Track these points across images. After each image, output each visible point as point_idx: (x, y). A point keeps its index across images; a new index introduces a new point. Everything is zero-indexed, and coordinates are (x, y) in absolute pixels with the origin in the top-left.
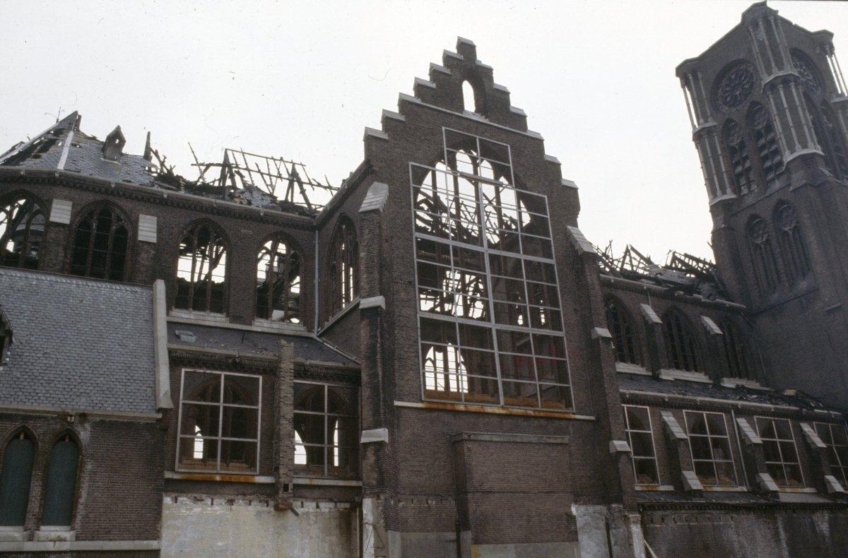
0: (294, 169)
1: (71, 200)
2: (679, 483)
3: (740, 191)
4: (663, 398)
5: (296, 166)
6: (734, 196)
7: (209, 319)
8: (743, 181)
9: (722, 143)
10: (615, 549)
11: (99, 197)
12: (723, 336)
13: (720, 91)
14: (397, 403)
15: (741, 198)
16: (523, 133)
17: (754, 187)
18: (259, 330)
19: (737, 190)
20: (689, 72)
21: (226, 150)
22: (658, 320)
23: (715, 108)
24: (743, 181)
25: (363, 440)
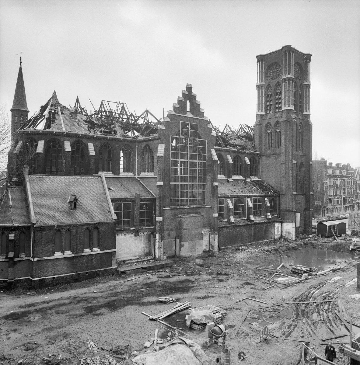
0: (123, 106)
1: (69, 141)
2: (229, 219)
3: (267, 112)
4: (228, 196)
5: (124, 105)
6: (265, 113)
7: (109, 174)
8: (269, 108)
9: (265, 92)
10: (210, 239)
11: (76, 139)
12: (250, 165)
13: (269, 71)
14: (164, 208)
15: (267, 114)
16: (203, 119)
17: (271, 112)
18: (121, 177)
19: (266, 111)
20: (261, 59)
21: (102, 101)
22: (232, 207)
23: (266, 77)
24: (269, 108)
25: (157, 220)
